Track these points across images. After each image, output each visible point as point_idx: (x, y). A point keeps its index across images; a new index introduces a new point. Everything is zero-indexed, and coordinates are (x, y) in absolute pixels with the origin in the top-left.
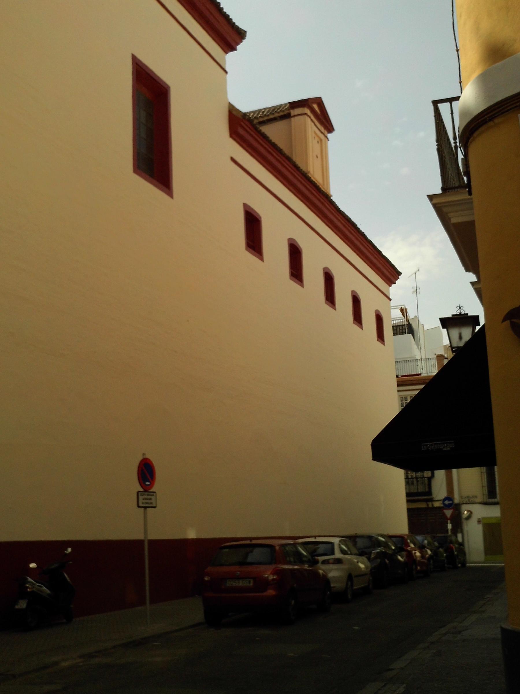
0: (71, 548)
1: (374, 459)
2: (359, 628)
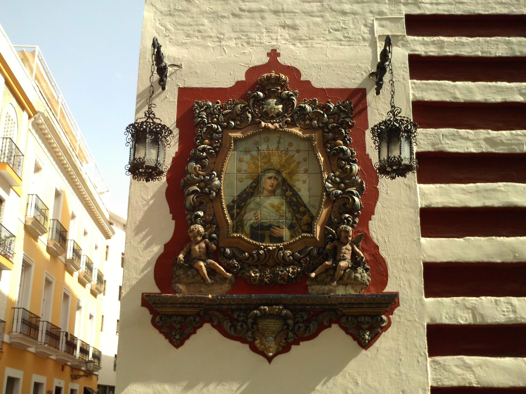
1: (178, 343)
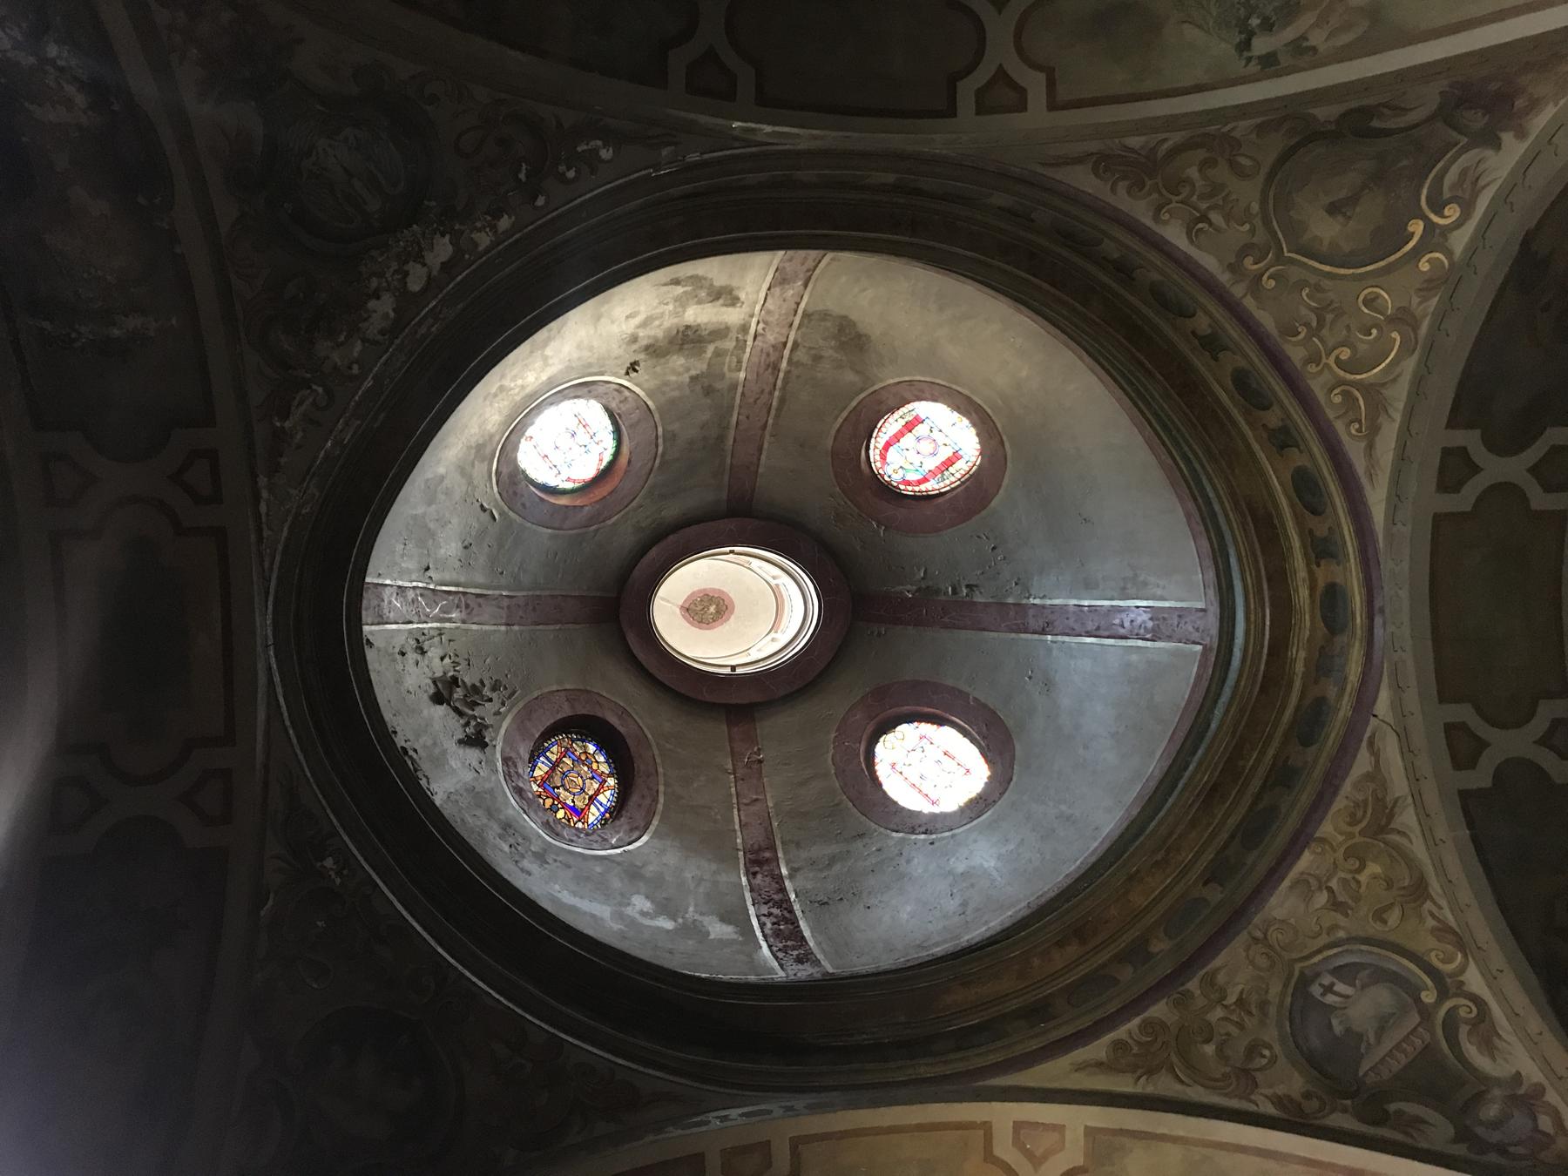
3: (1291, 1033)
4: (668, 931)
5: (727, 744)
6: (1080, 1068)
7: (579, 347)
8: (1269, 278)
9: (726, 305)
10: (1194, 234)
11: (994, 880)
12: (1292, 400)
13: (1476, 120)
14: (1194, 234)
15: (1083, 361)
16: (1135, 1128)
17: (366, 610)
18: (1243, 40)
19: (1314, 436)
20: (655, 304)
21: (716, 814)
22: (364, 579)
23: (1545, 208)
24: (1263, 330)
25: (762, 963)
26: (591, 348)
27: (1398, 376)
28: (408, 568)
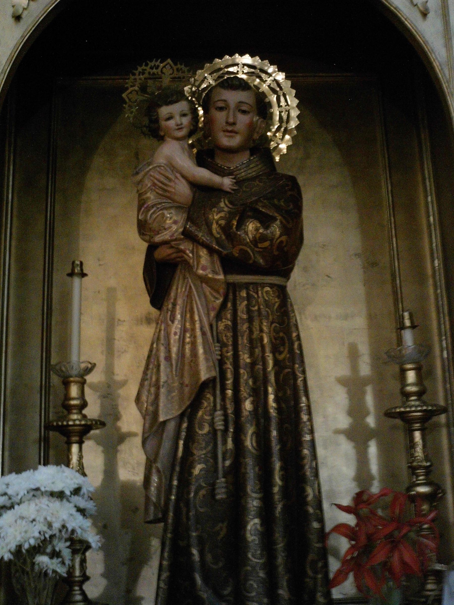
0: (285, 154)
2: (70, 428)
3: (146, 408)
4: (380, 529)
5: (387, 245)
6: (210, 293)
7: (155, 368)
8: (267, 312)
9: (80, 371)
10: (270, 312)
11: (427, 555)
12: (220, 268)
13: (265, 301)
14: (270, 312)
15: (305, 381)
16: (54, 296)
17: (305, 269)
18: (290, 143)
19: (415, 33)
20: (165, 69)
21: (396, 179)
22: (51, 430)
23: (154, 525)
24: (274, 464)
25: (203, 472)
26: (360, 359)
27: (182, 218)
28: (202, 450)
